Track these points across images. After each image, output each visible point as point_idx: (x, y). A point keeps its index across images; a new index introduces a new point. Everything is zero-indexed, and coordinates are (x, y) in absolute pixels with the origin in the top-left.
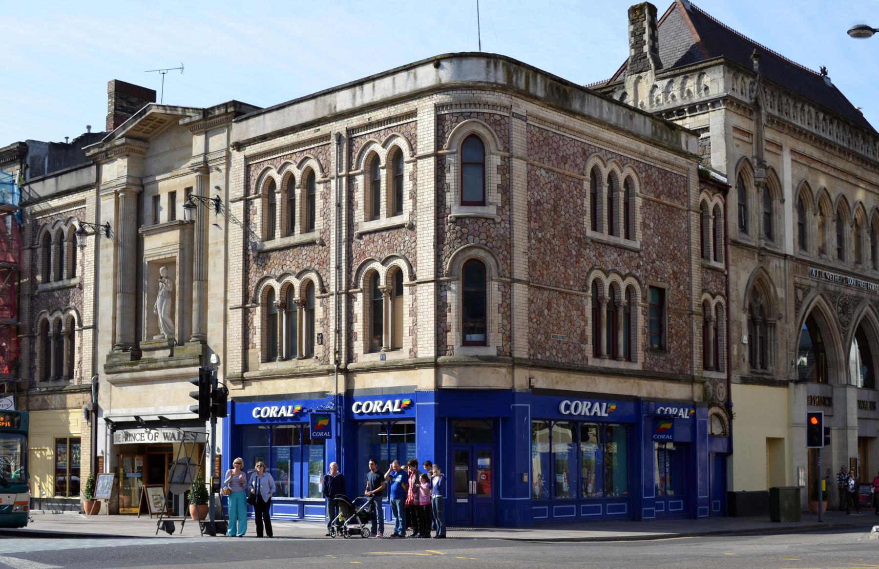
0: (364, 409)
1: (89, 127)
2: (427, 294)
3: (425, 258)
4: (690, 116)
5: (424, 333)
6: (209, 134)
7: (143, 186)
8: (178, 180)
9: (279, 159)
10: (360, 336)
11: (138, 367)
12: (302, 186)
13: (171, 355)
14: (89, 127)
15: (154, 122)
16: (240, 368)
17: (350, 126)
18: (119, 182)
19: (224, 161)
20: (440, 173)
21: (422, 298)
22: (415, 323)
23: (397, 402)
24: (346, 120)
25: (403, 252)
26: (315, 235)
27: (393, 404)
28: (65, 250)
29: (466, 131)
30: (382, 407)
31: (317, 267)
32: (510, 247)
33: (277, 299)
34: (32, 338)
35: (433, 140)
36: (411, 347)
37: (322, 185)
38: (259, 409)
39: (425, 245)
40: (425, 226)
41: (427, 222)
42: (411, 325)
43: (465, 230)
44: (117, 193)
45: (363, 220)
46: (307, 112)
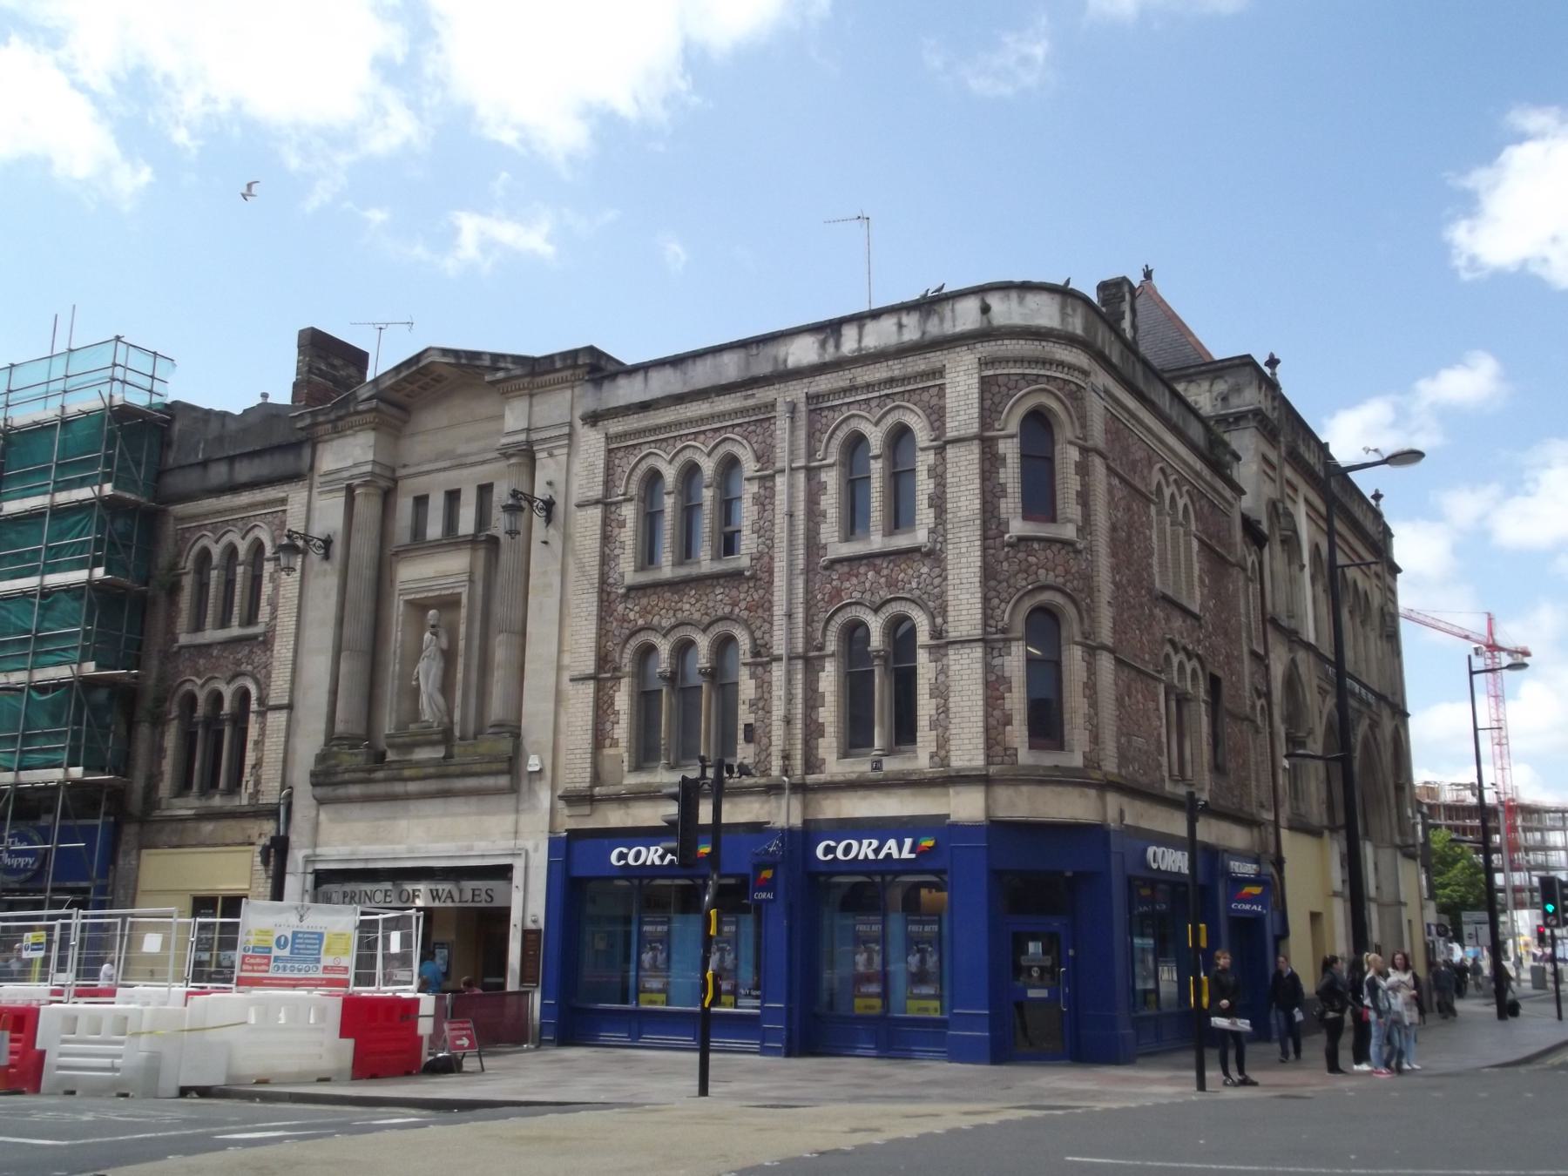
0: (631, 861)
1: (265, 396)
2: (968, 661)
3: (965, 602)
4: (1510, 667)
5: (962, 725)
6: (535, 400)
7: (395, 481)
8: (465, 472)
9: (671, 442)
10: (830, 730)
11: (380, 775)
12: (715, 484)
13: (449, 756)
14: (265, 396)
15: (428, 380)
16: (588, 780)
17: (813, 390)
18: (356, 471)
19: (566, 442)
20: (987, 465)
21: (958, 667)
22: (944, 709)
23: (908, 842)
24: (805, 381)
25: (917, 593)
26: (258, 629)
27: (900, 848)
28: (239, 579)
29: (1030, 403)
30: (877, 851)
31: (745, 614)
32: (1091, 590)
33: (201, 711)
34: (159, 722)
35: (976, 415)
36: (934, 749)
37: (272, 563)
38: (625, 850)
39: (964, 581)
40: (964, 550)
41: (968, 544)
42: (933, 712)
43: (1032, 559)
44: (350, 490)
45: (837, 539)
46: (730, 368)
